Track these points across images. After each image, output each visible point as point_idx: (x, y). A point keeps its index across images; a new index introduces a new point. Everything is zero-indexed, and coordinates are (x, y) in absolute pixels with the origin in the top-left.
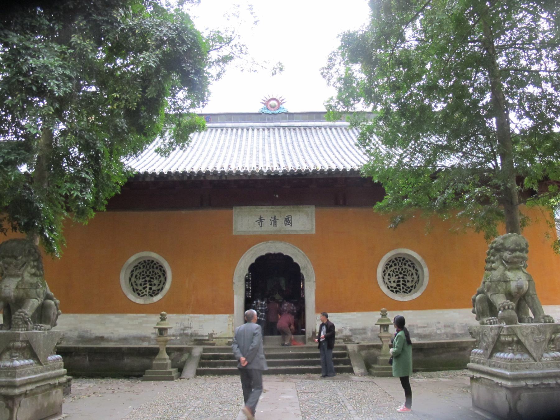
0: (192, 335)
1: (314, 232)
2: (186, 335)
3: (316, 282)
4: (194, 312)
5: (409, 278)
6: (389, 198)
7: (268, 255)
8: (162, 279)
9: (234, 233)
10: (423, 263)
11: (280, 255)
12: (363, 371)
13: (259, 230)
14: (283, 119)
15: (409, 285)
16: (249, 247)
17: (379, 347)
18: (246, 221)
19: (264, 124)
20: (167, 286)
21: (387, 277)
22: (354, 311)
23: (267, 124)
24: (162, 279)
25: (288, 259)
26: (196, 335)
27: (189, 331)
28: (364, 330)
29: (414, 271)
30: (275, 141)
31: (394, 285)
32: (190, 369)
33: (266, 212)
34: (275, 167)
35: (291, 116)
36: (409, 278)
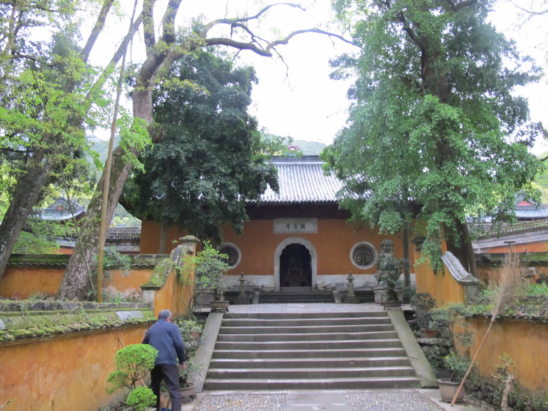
0: (252, 286)
1: (317, 232)
2: (250, 286)
3: (318, 259)
4: (253, 274)
5: (367, 257)
6: (353, 218)
7: (293, 244)
8: (236, 257)
9: (274, 233)
10: (375, 249)
11: (299, 244)
12: (339, 301)
13: (288, 232)
14: (299, 160)
15: (367, 261)
16: (282, 240)
17: (347, 292)
18: (280, 226)
19: (287, 163)
20: (239, 260)
21: (355, 256)
22: (337, 274)
23: (289, 163)
24: (236, 257)
25: (303, 247)
26: (255, 286)
27: (251, 284)
28: (342, 284)
29: (370, 254)
30: (294, 176)
31: (360, 261)
32: (256, 300)
33: (291, 222)
34: (297, 199)
35: (304, 158)
36: (367, 257)
